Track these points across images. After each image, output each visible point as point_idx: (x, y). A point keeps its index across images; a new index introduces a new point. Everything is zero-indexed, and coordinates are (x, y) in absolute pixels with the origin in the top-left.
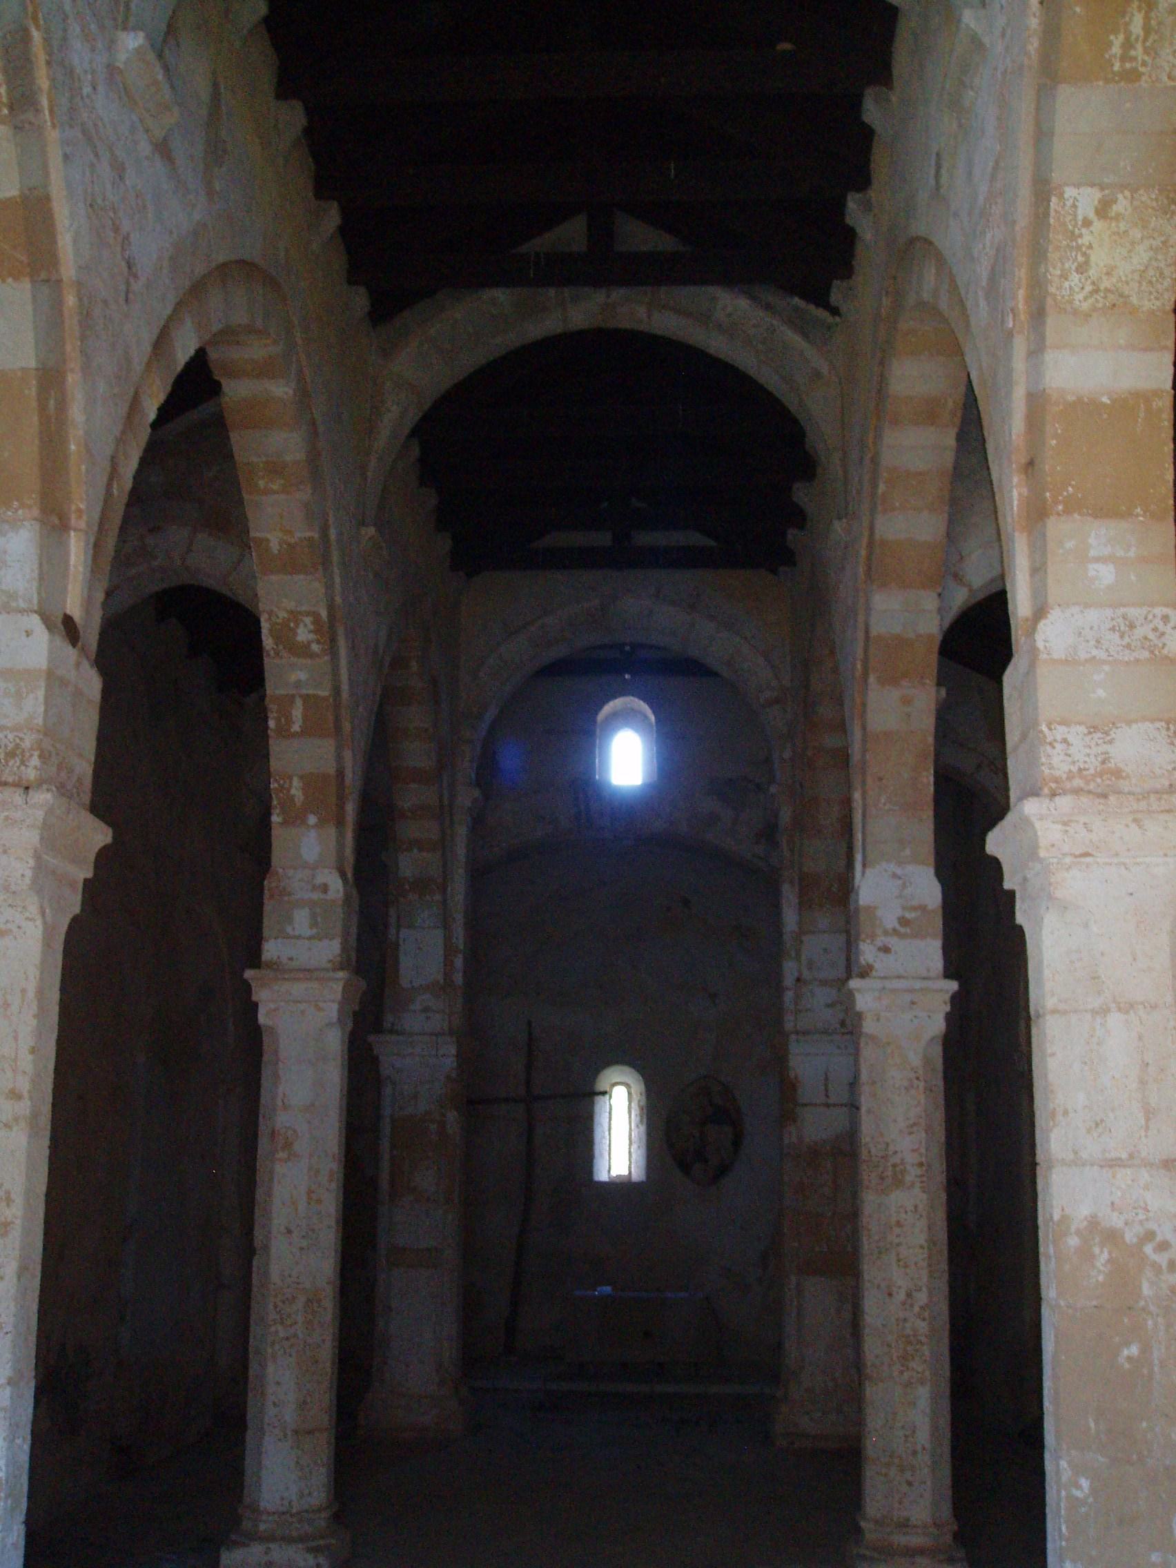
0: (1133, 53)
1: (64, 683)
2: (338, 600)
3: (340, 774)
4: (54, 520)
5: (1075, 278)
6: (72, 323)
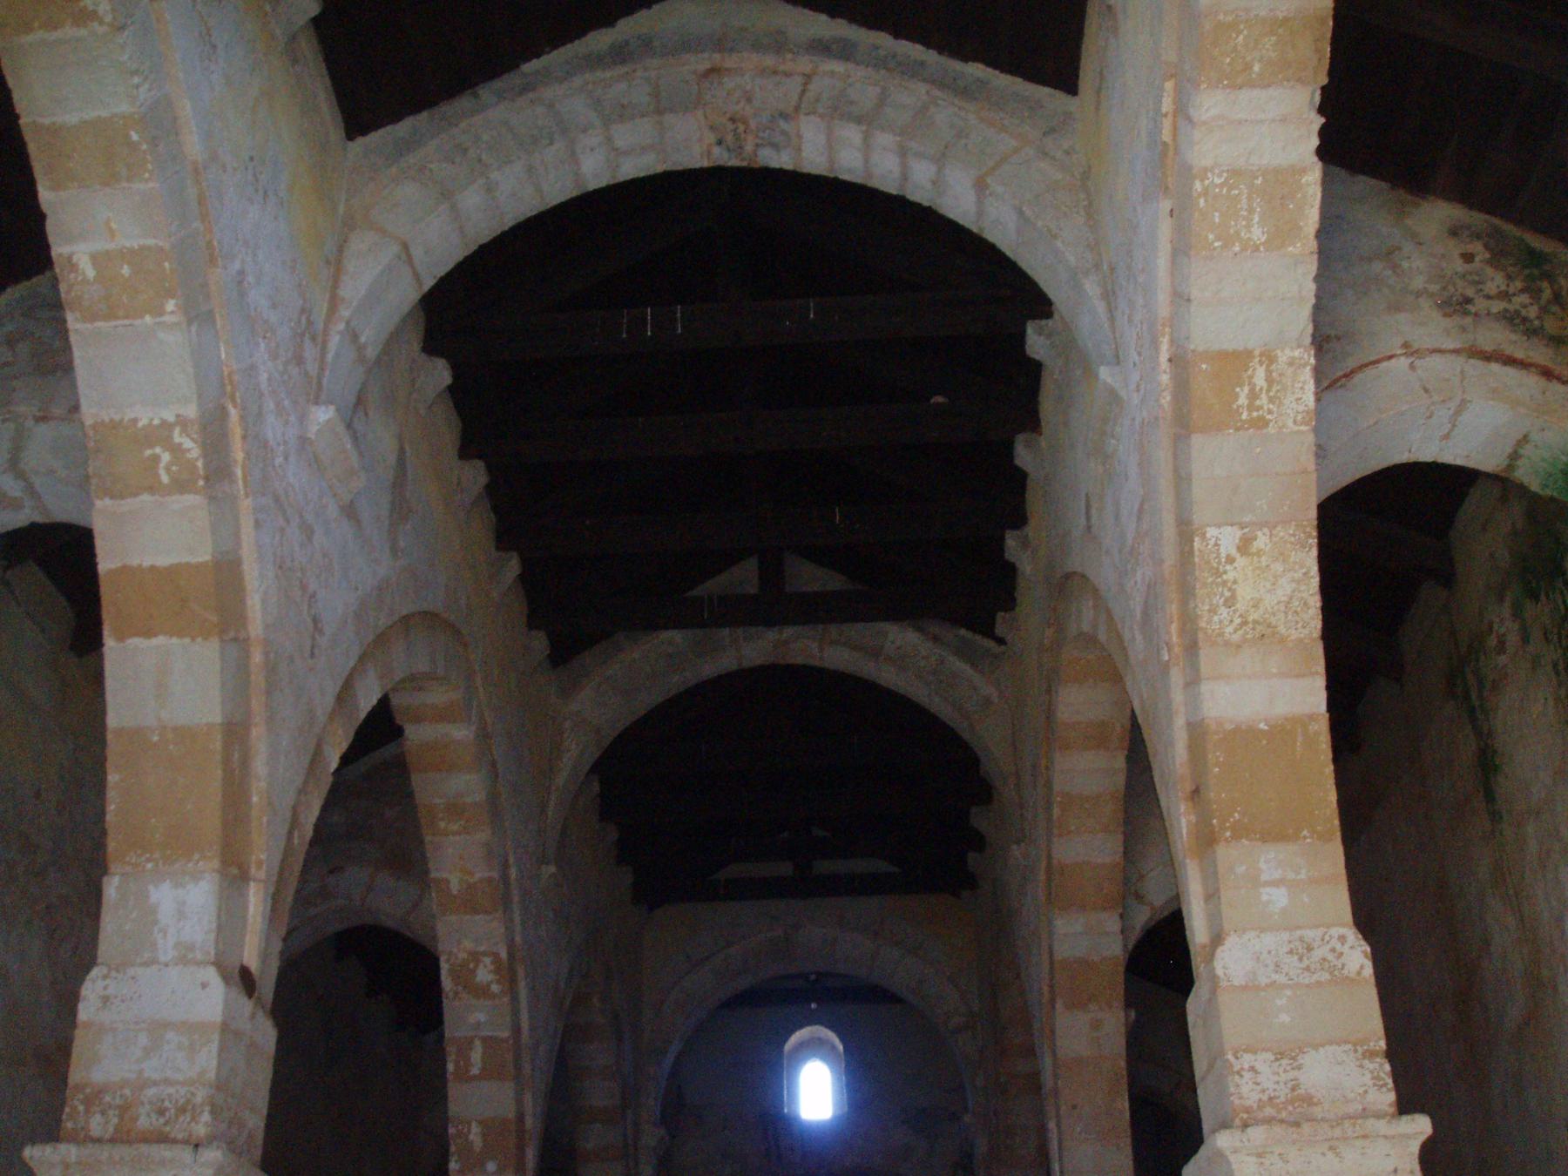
0: (1258, 403)
1: (238, 1034)
2: (518, 939)
3: (520, 1118)
4: (234, 873)
5: (1224, 612)
6: (258, 679)
